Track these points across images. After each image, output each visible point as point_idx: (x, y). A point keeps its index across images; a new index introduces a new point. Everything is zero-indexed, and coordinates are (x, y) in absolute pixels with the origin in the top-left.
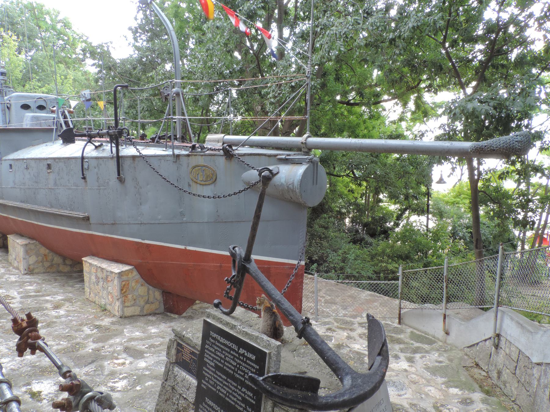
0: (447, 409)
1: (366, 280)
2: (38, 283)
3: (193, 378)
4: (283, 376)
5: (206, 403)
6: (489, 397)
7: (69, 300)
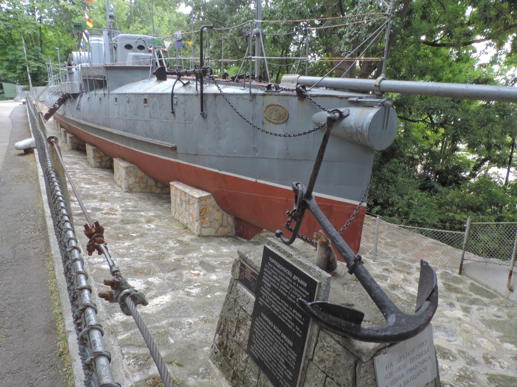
0: (497, 362)
1: (430, 227)
2: (135, 200)
4: (329, 304)
5: (261, 317)
7: (159, 217)
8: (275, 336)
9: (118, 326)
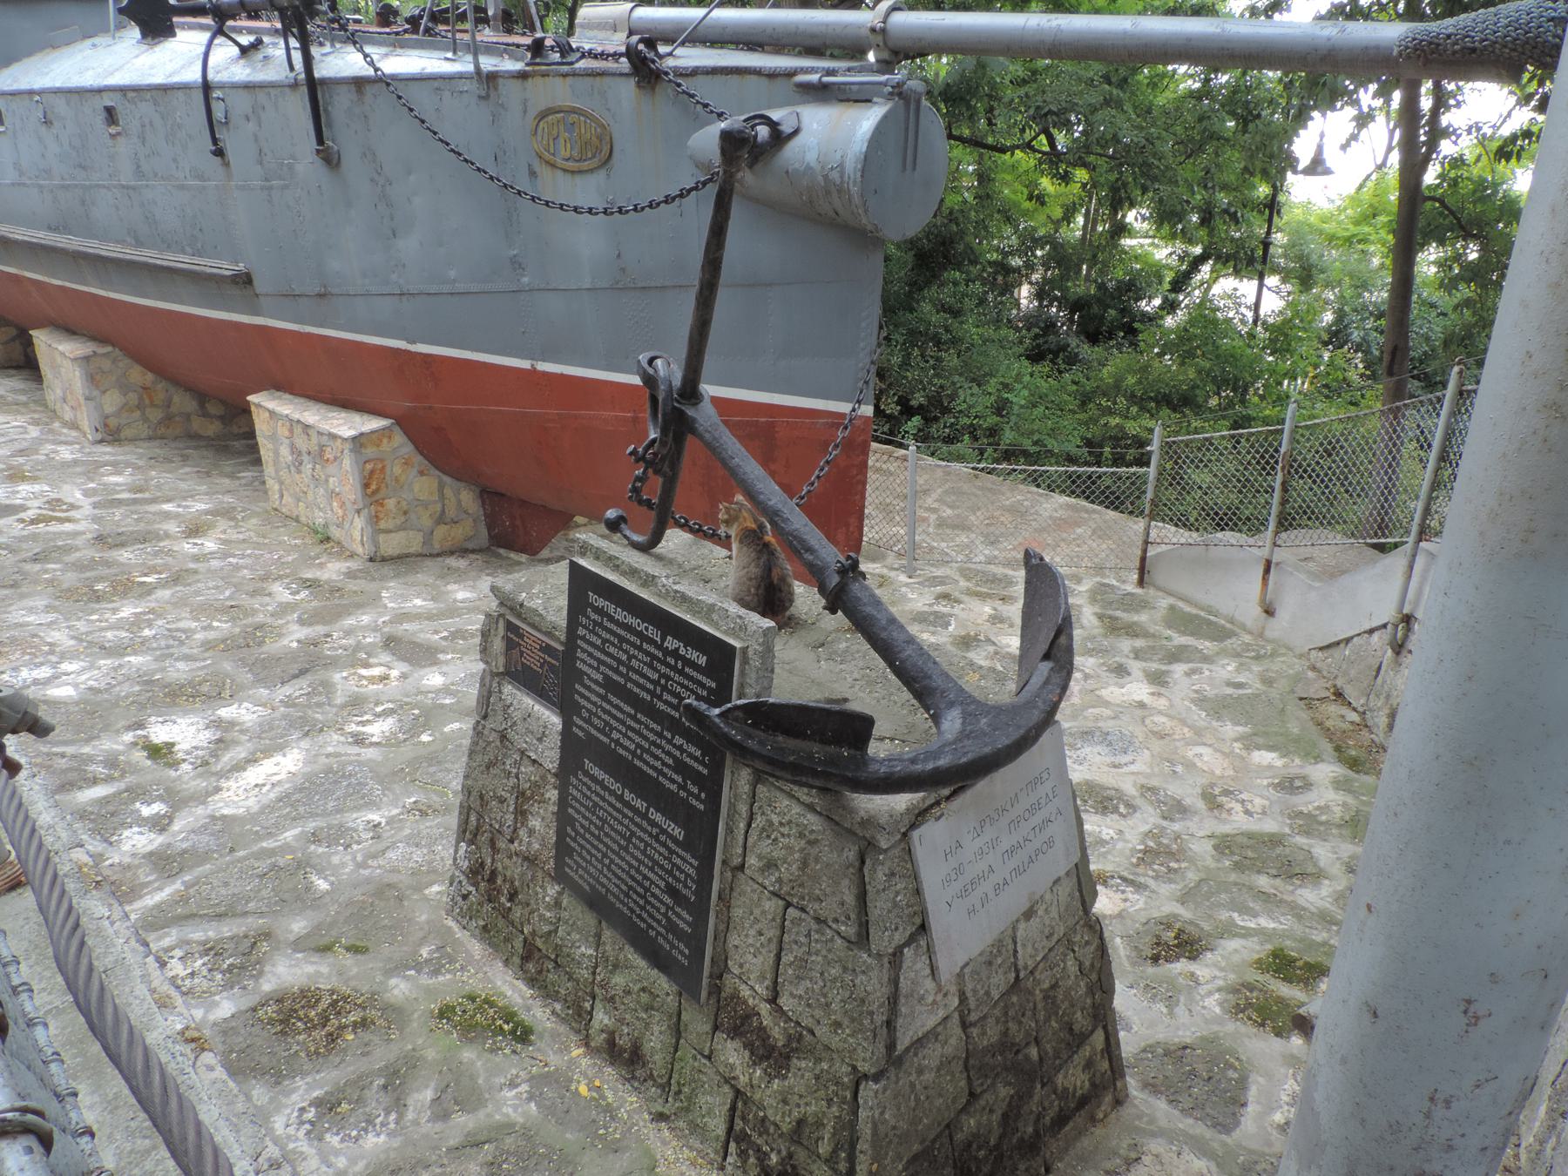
0: (1237, 801)
1: (1058, 464)
2: (136, 468)
3: (552, 710)
6: (1356, 776)
7: (227, 513)
8: (632, 820)
9: (139, 866)
